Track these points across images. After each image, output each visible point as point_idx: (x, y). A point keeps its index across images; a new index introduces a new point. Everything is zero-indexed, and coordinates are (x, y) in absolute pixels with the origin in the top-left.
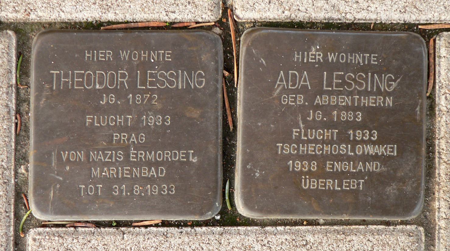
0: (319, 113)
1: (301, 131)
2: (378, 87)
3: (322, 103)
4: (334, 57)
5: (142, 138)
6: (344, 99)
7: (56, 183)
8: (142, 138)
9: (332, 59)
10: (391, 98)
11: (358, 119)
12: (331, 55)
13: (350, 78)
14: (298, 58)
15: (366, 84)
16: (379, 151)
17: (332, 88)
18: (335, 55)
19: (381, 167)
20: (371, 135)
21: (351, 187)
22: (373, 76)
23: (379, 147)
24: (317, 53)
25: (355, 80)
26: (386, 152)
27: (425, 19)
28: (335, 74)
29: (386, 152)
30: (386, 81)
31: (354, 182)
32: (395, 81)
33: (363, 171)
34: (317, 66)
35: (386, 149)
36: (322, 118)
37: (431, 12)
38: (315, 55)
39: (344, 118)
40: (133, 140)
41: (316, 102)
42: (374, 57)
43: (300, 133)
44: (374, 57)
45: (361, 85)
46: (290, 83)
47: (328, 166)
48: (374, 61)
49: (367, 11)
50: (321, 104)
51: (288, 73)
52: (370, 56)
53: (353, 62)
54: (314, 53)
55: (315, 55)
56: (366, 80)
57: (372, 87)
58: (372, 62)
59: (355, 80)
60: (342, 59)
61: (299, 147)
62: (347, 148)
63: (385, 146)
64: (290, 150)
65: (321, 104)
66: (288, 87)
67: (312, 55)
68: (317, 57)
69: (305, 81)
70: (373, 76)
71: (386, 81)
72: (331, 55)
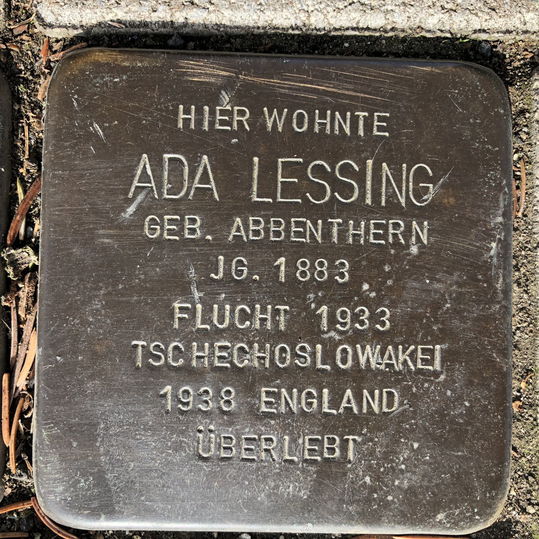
0: (241, 261)
1: (195, 308)
2: (391, 196)
3: (247, 236)
4: (280, 119)
5: (309, 400)
6: (303, 225)
7: (197, 421)
8: (309, 400)
9: (275, 124)
10: (426, 223)
11: (361, 325)
12: (271, 113)
13: (319, 171)
14: (187, 121)
15: (359, 188)
16: (397, 361)
17: (274, 198)
18: (280, 114)
19: (401, 404)
20: (375, 318)
21: (326, 455)
22: (377, 169)
23: (396, 349)
24: (236, 108)
25: (330, 178)
26: (415, 363)
27: (504, 29)
28: (282, 162)
29: (415, 363)
30: (411, 180)
31: (332, 441)
32: (433, 181)
33: (355, 411)
34: (235, 140)
35: (413, 355)
36: (250, 274)
37: (519, 9)
38: (230, 113)
39: (303, 274)
40: (350, 405)
41: (233, 232)
42: (380, 119)
43: (193, 312)
44: (380, 119)
45: (346, 190)
46: (166, 186)
47: (264, 398)
48: (380, 129)
49: (361, 8)
50: (245, 239)
51: (161, 159)
52: (371, 116)
53: (328, 132)
54: (229, 108)
55: (230, 113)
56: (361, 178)
57: (376, 195)
58: (376, 132)
59: (330, 178)
60: (300, 124)
61: (189, 348)
62: (313, 355)
63: (412, 347)
64: (166, 359)
65: (245, 239)
66: (160, 194)
67: (223, 112)
68: (236, 118)
69: (205, 179)
70: (377, 169)
71: (411, 180)
72: (271, 113)
